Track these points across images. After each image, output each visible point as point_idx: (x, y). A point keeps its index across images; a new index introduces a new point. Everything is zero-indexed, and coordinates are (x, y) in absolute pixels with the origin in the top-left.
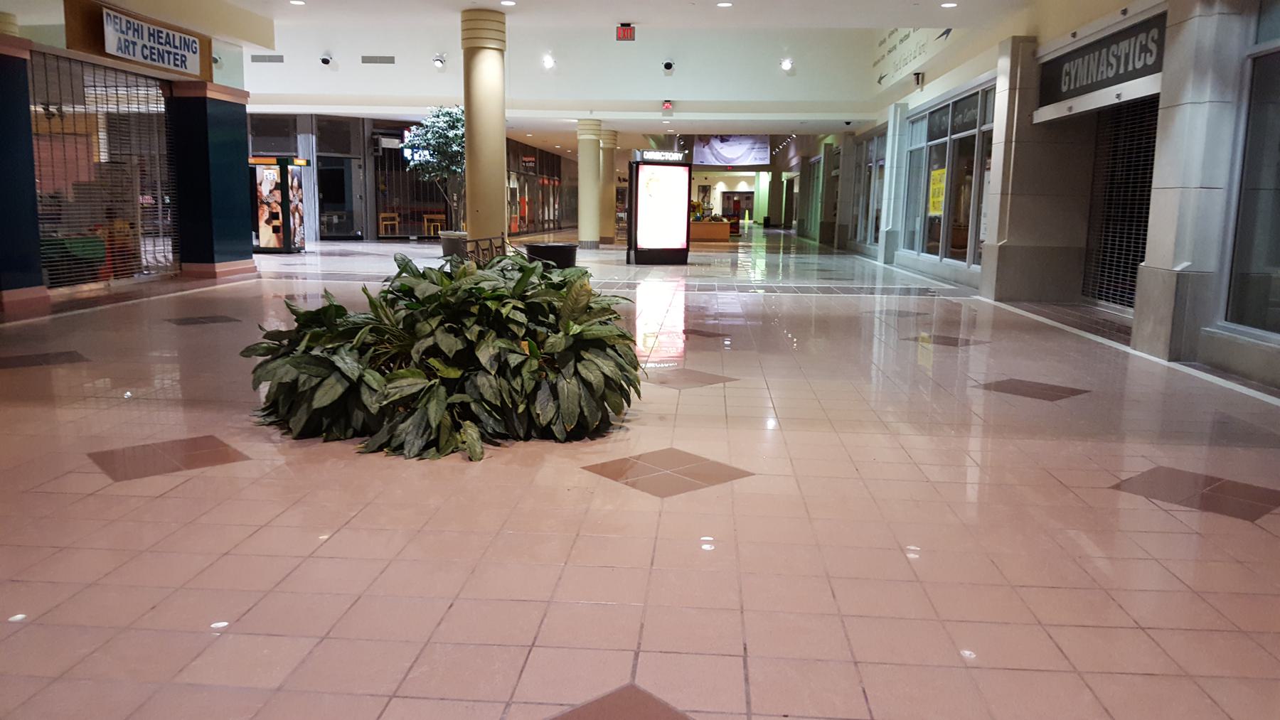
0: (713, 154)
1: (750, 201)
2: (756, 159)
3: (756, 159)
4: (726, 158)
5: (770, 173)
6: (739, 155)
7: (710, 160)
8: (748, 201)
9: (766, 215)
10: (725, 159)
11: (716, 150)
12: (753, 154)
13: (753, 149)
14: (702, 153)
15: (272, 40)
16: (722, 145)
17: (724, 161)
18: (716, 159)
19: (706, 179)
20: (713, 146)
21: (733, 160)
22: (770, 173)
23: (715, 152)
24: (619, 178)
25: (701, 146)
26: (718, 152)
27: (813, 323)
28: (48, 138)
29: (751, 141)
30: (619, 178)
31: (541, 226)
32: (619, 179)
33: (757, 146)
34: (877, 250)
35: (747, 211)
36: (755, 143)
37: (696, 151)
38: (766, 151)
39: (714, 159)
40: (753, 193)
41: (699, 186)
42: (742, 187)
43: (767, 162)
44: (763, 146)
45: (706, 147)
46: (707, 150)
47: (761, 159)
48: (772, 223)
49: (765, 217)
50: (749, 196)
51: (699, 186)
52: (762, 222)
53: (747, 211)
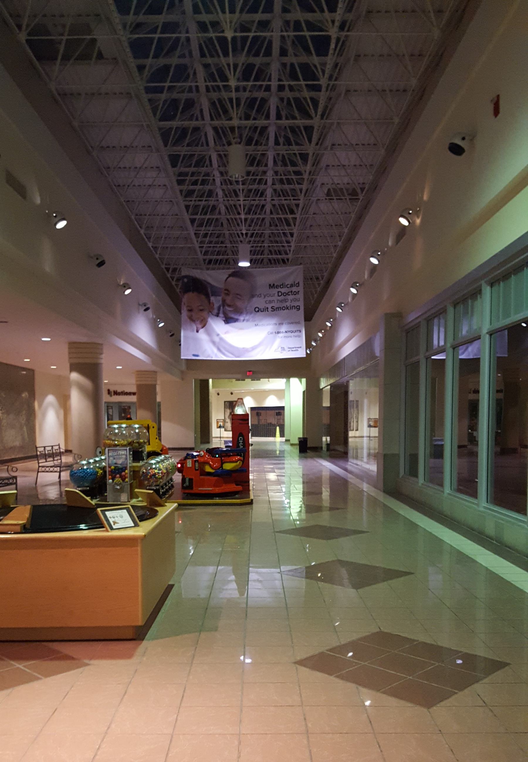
0: (214, 343)
1: (282, 416)
2: (283, 349)
3: (283, 349)
4: (237, 348)
5: (304, 380)
6: (256, 343)
7: (209, 352)
8: (279, 417)
9: (301, 436)
10: (232, 349)
11: (218, 335)
12: (279, 341)
13: (278, 333)
14: (197, 341)
15: (526, 510)
16: (228, 327)
17: (232, 354)
18: (219, 349)
19: (232, 394)
20: (213, 330)
21: (246, 351)
22: (304, 380)
23: (216, 339)
24: (109, 390)
25: (193, 331)
26: (221, 339)
27: (60, 57)
28: (368, 435)
29: (273, 321)
30: (109, 390)
31: (117, 439)
32: (109, 392)
33: (284, 328)
34: (101, 364)
35: (278, 428)
36: (281, 324)
37: (184, 336)
38: (299, 336)
39: (215, 350)
40: (283, 408)
41: (225, 402)
42: (271, 402)
43: (301, 353)
44: (293, 328)
45: (201, 331)
46: (202, 335)
47: (291, 349)
48: (309, 445)
49: (299, 438)
50: (279, 411)
51: (225, 402)
52: (297, 442)
53: (278, 428)
